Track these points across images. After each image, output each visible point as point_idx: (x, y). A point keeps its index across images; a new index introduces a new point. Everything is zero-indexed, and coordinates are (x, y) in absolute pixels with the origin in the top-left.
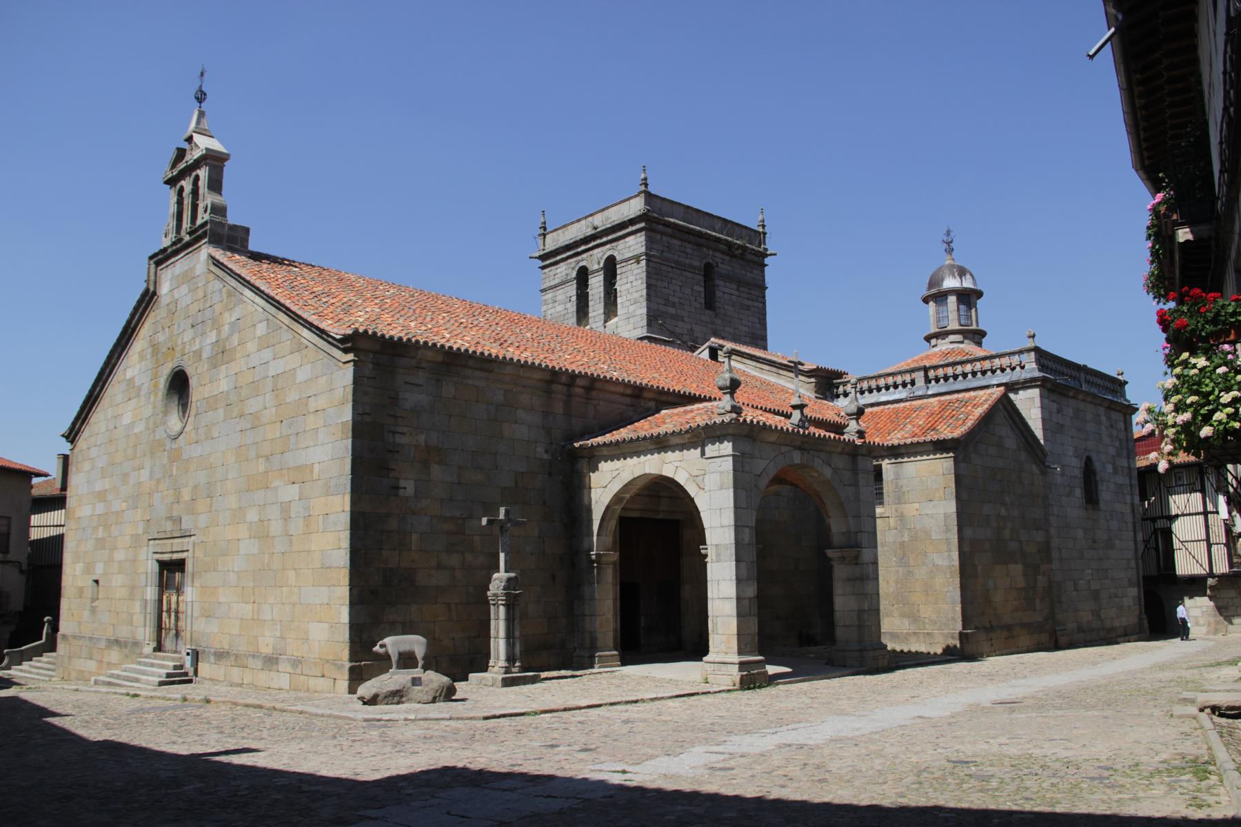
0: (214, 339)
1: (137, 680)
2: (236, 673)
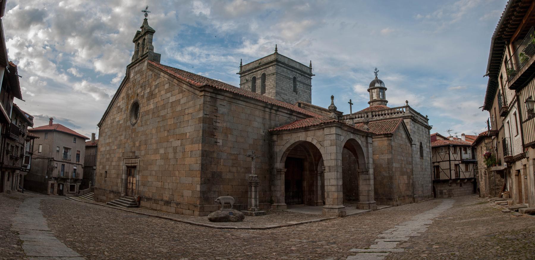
0: (149, 91)
2: (154, 206)
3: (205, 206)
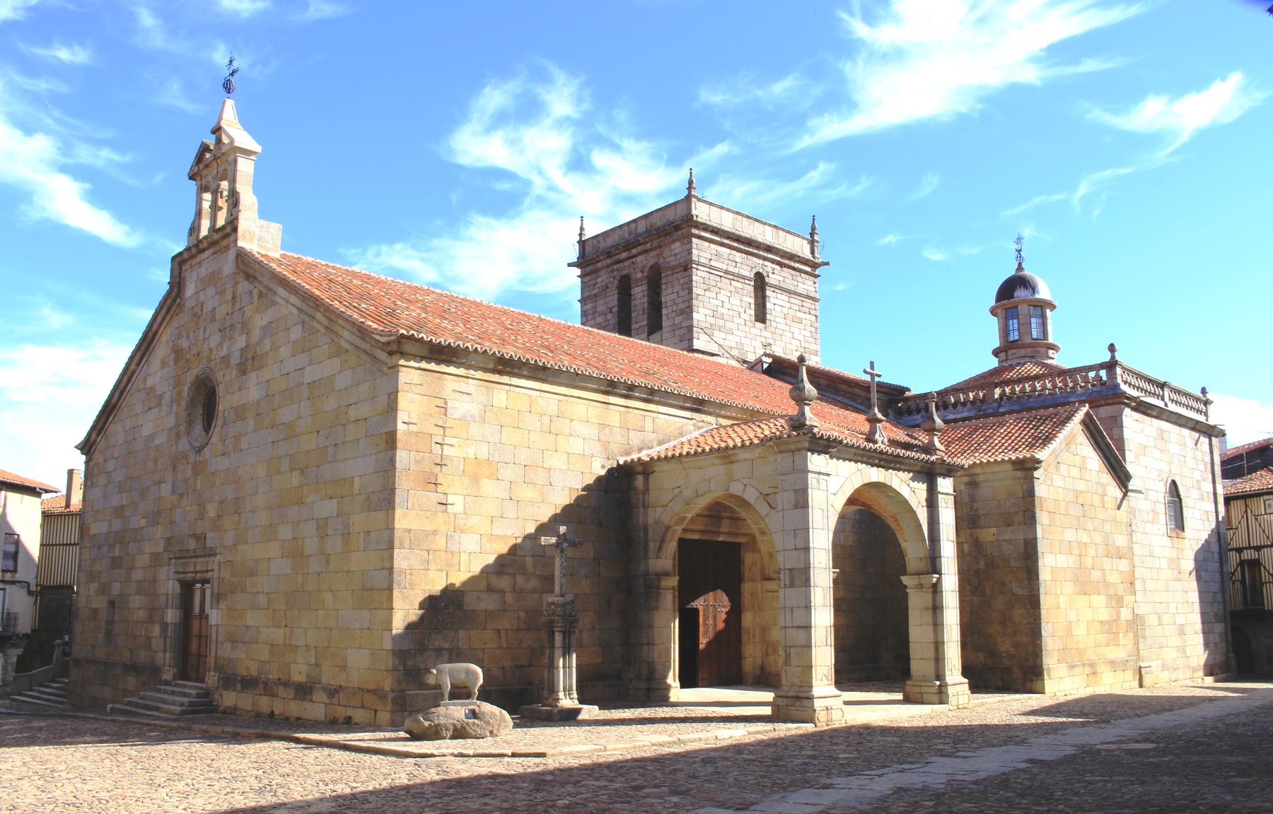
1: (157, 709)
3: (410, 695)
